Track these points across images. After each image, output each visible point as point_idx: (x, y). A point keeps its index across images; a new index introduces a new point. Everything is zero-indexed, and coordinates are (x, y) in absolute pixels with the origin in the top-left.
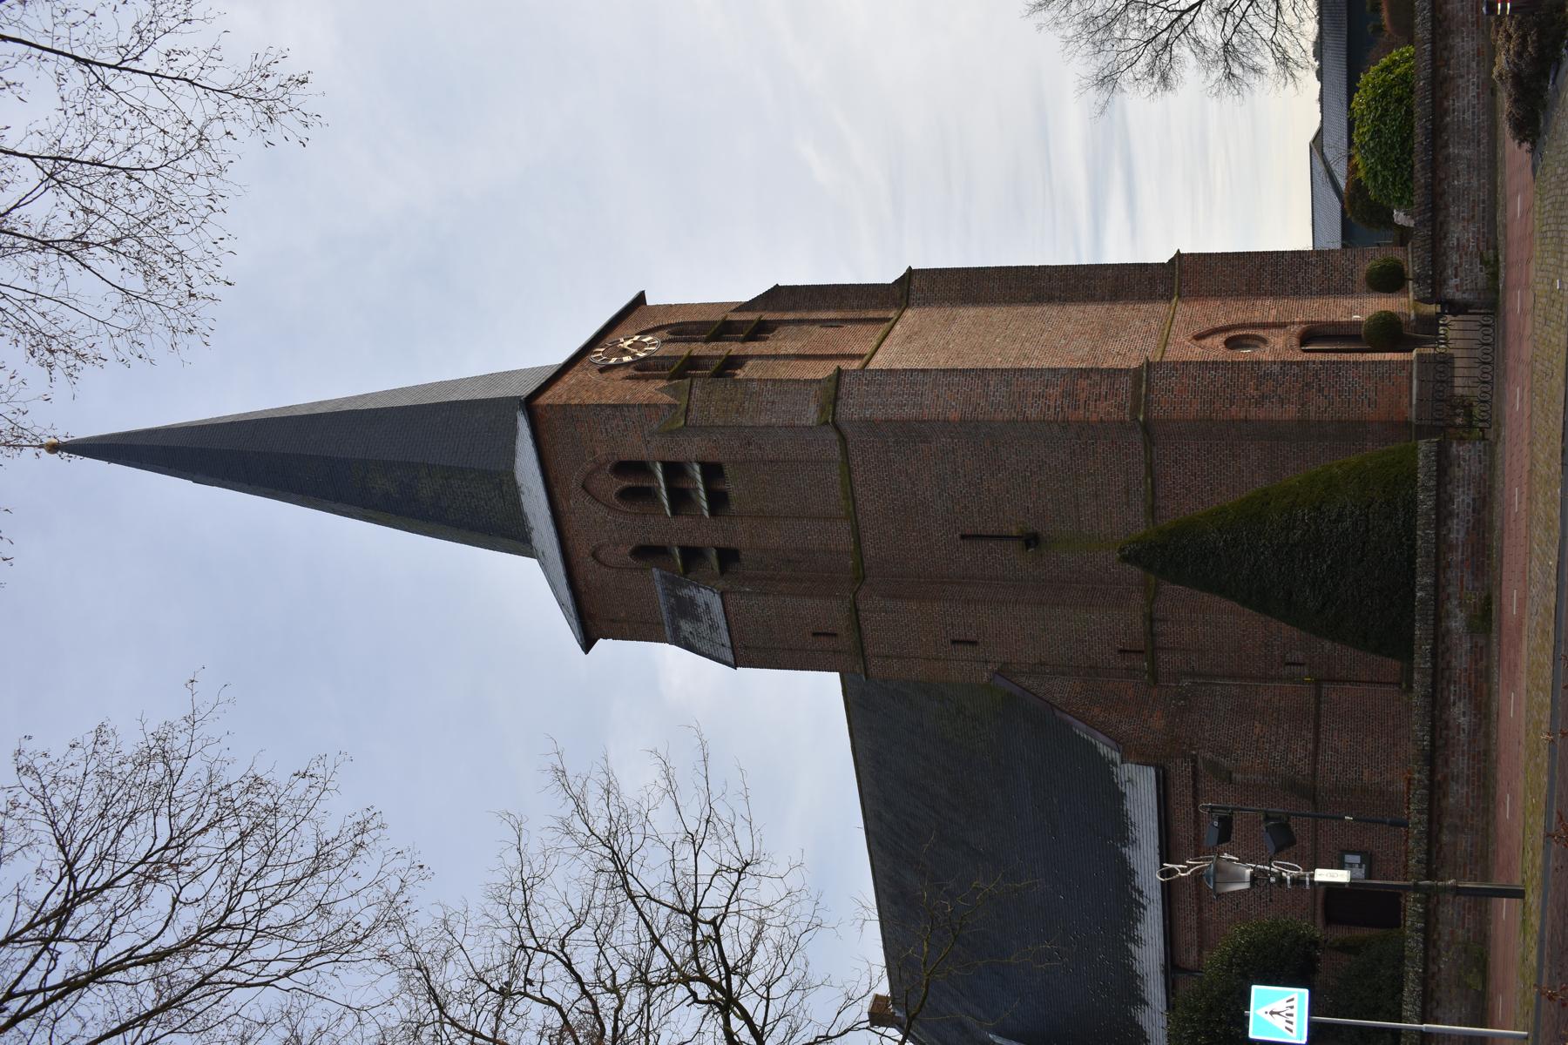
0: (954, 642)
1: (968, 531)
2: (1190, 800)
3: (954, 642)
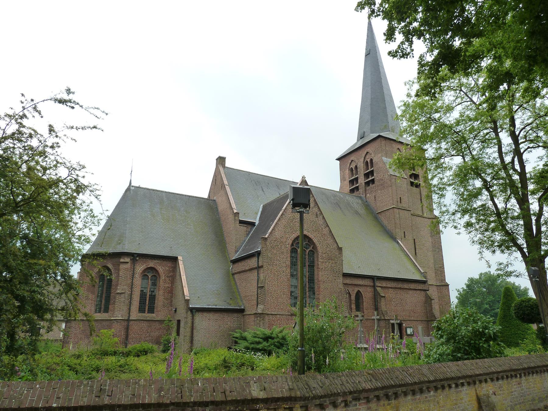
0: (404, 232)
1: (416, 241)
2: (419, 288)
3: (404, 232)
